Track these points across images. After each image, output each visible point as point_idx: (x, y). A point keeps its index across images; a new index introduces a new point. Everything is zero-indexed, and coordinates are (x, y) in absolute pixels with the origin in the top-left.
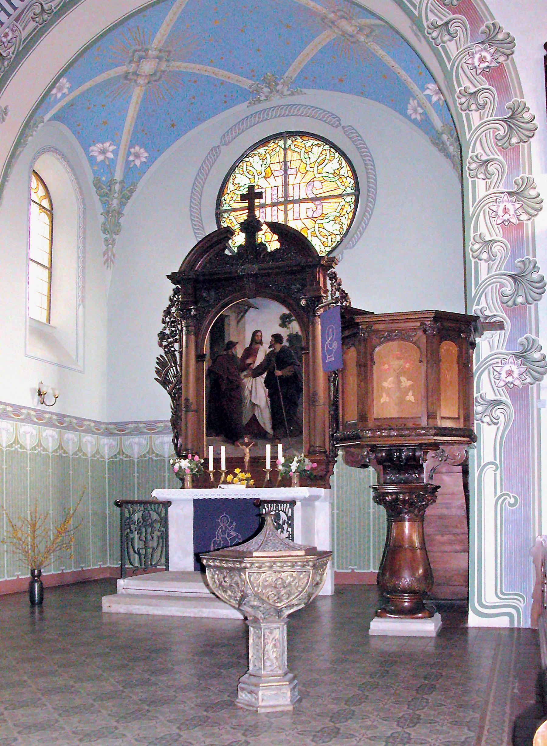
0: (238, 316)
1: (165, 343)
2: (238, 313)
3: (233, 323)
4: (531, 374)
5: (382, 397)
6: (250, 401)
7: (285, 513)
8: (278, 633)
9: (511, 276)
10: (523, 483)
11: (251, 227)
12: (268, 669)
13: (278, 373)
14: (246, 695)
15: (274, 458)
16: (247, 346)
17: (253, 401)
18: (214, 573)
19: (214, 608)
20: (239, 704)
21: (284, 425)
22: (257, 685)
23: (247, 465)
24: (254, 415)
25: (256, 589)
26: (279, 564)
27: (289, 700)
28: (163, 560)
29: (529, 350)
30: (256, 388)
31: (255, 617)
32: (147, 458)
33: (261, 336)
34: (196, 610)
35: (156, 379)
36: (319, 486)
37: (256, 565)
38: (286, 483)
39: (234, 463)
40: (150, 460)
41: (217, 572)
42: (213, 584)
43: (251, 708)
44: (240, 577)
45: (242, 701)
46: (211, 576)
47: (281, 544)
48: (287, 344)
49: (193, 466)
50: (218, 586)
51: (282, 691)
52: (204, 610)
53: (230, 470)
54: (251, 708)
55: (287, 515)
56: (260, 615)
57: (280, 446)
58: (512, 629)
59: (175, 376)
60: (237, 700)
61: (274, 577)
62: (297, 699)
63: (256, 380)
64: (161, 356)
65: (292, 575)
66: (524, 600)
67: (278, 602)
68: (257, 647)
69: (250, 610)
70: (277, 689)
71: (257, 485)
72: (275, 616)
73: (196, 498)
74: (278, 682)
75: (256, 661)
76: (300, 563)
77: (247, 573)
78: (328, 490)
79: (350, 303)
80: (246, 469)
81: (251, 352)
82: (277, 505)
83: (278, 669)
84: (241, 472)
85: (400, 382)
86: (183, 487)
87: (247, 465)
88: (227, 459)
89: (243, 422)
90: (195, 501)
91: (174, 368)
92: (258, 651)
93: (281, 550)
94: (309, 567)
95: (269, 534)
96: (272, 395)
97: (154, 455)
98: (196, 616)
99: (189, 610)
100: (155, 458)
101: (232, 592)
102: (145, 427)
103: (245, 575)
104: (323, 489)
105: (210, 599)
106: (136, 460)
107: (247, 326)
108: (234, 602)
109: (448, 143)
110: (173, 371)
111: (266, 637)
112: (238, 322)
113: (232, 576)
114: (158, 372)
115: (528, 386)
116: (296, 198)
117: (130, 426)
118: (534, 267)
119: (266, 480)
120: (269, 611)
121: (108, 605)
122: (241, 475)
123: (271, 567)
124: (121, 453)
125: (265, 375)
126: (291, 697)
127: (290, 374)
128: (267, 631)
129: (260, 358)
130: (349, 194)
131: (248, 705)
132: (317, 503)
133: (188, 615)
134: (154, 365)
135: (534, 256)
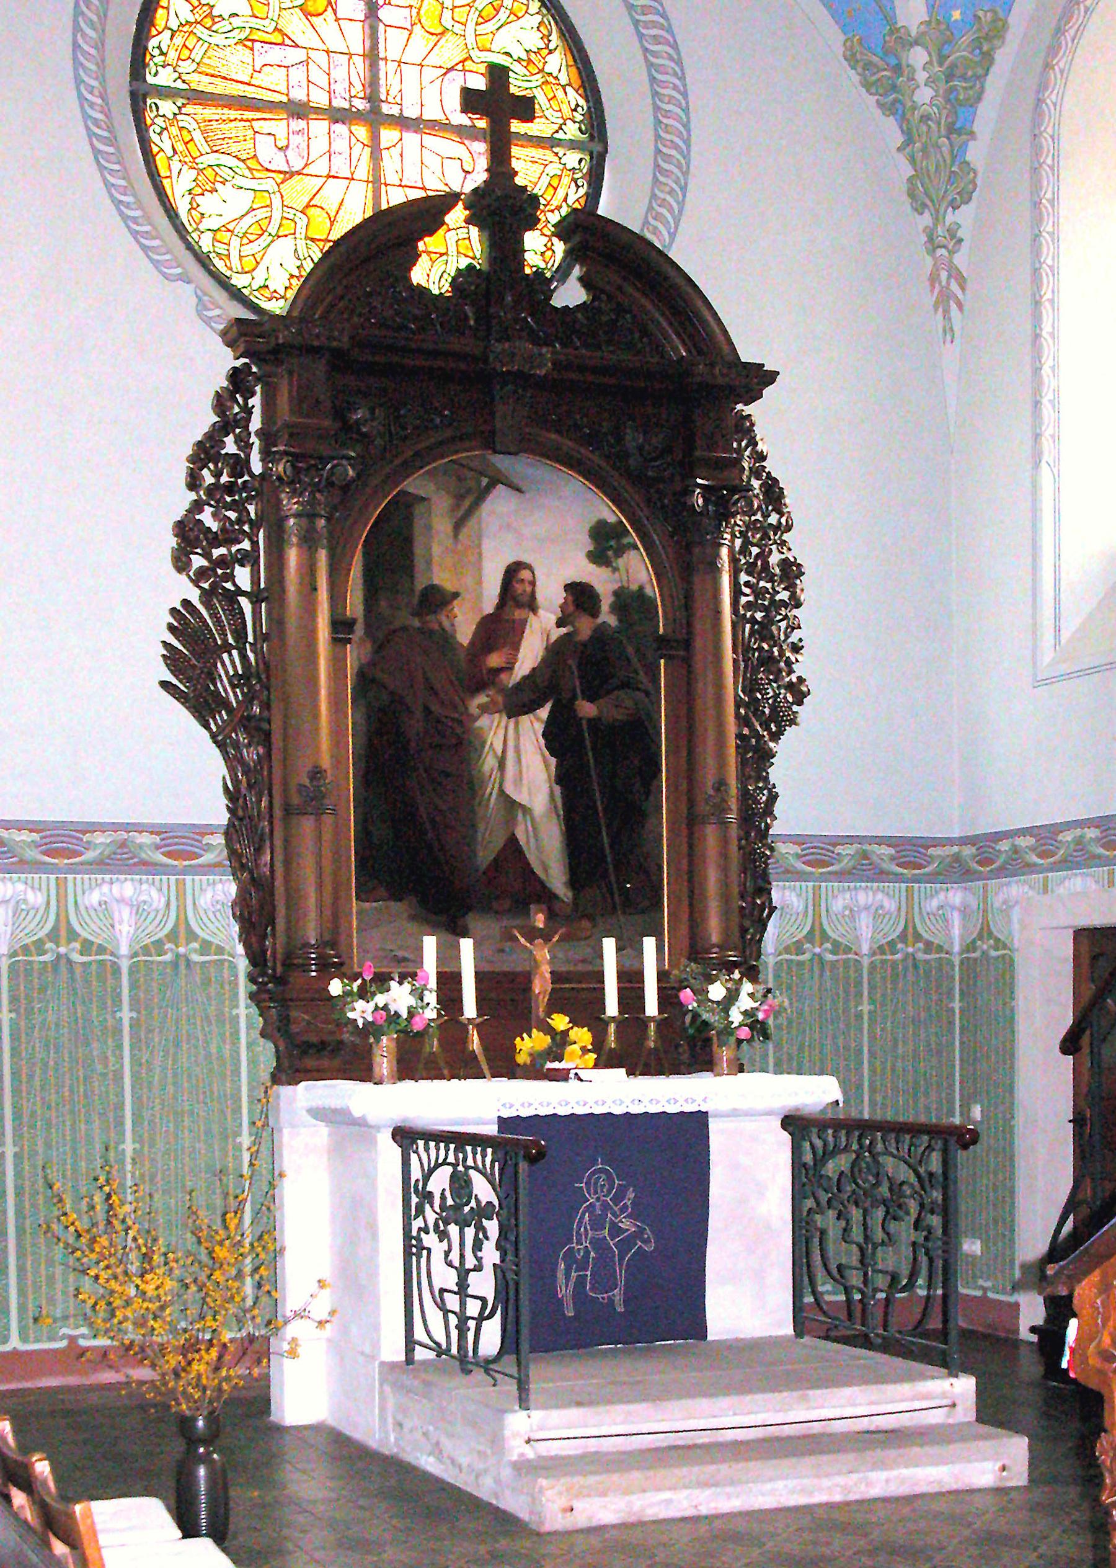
0: (455, 508)
1: (198, 562)
2: (459, 498)
3: (442, 524)
6: (501, 792)
11: (503, 209)
13: (587, 709)
15: (631, 981)
16: (489, 607)
17: (510, 790)
21: (605, 875)
24: (513, 841)
30: (517, 750)
32: (806, 957)
33: (533, 583)
35: (165, 685)
39: (506, 997)
40: (910, 963)
48: (612, 621)
52: (873, 1475)
57: (467, 946)
59: (236, 681)
63: (517, 724)
64: (186, 603)
79: (789, 517)
81: (500, 629)
88: (479, 976)
89: (479, 859)
91: (235, 653)
96: (569, 780)
97: (196, 945)
99: (826, 1482)
100: (76, 957)
102: (892, 858)
106: (866, 962)
107: (488, 546)
109: (921, 76)
110: (230, 663)
112: (458, 527)
114: (172, 659)
116: (411, 112)
117: (100, 838)
121: (563, 1502)
124: (63, 933)
125: (544, 713)
127: (619, 715)
129: (530, 655)
130: (573, 145)
134: (154, 633)
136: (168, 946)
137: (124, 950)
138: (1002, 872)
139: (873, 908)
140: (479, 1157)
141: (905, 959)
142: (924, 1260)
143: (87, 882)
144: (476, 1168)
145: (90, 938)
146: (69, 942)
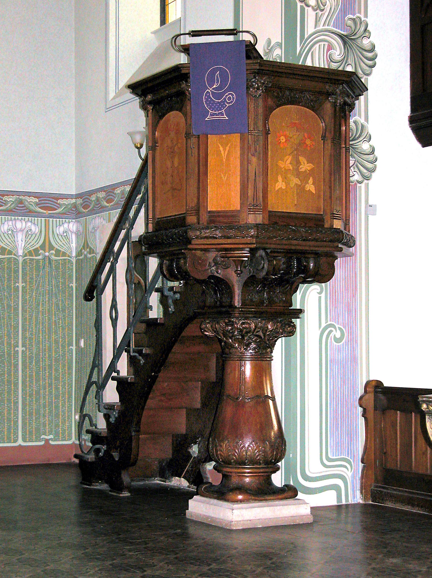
4: (359, 170)
5: (278, 181)
9: (341, 36)
10: (349, 311)
29: (360, 136)
58: (339, 507)
66: (351, 468)
85: (298, 163)
97: (53, 252)
100: (53, 257)
102: (37, 204)
106: (21, 260)
115: (356, 184)
117: (65, 202)
118: (365, 30)
135: (366, 16)
136: (41, 251)
137: (21, 252)
138: (93, 212)
139: (25, 231)
141: (44, 259)
143: (61, 221)
145: (5, 246)
146: (50, 250)
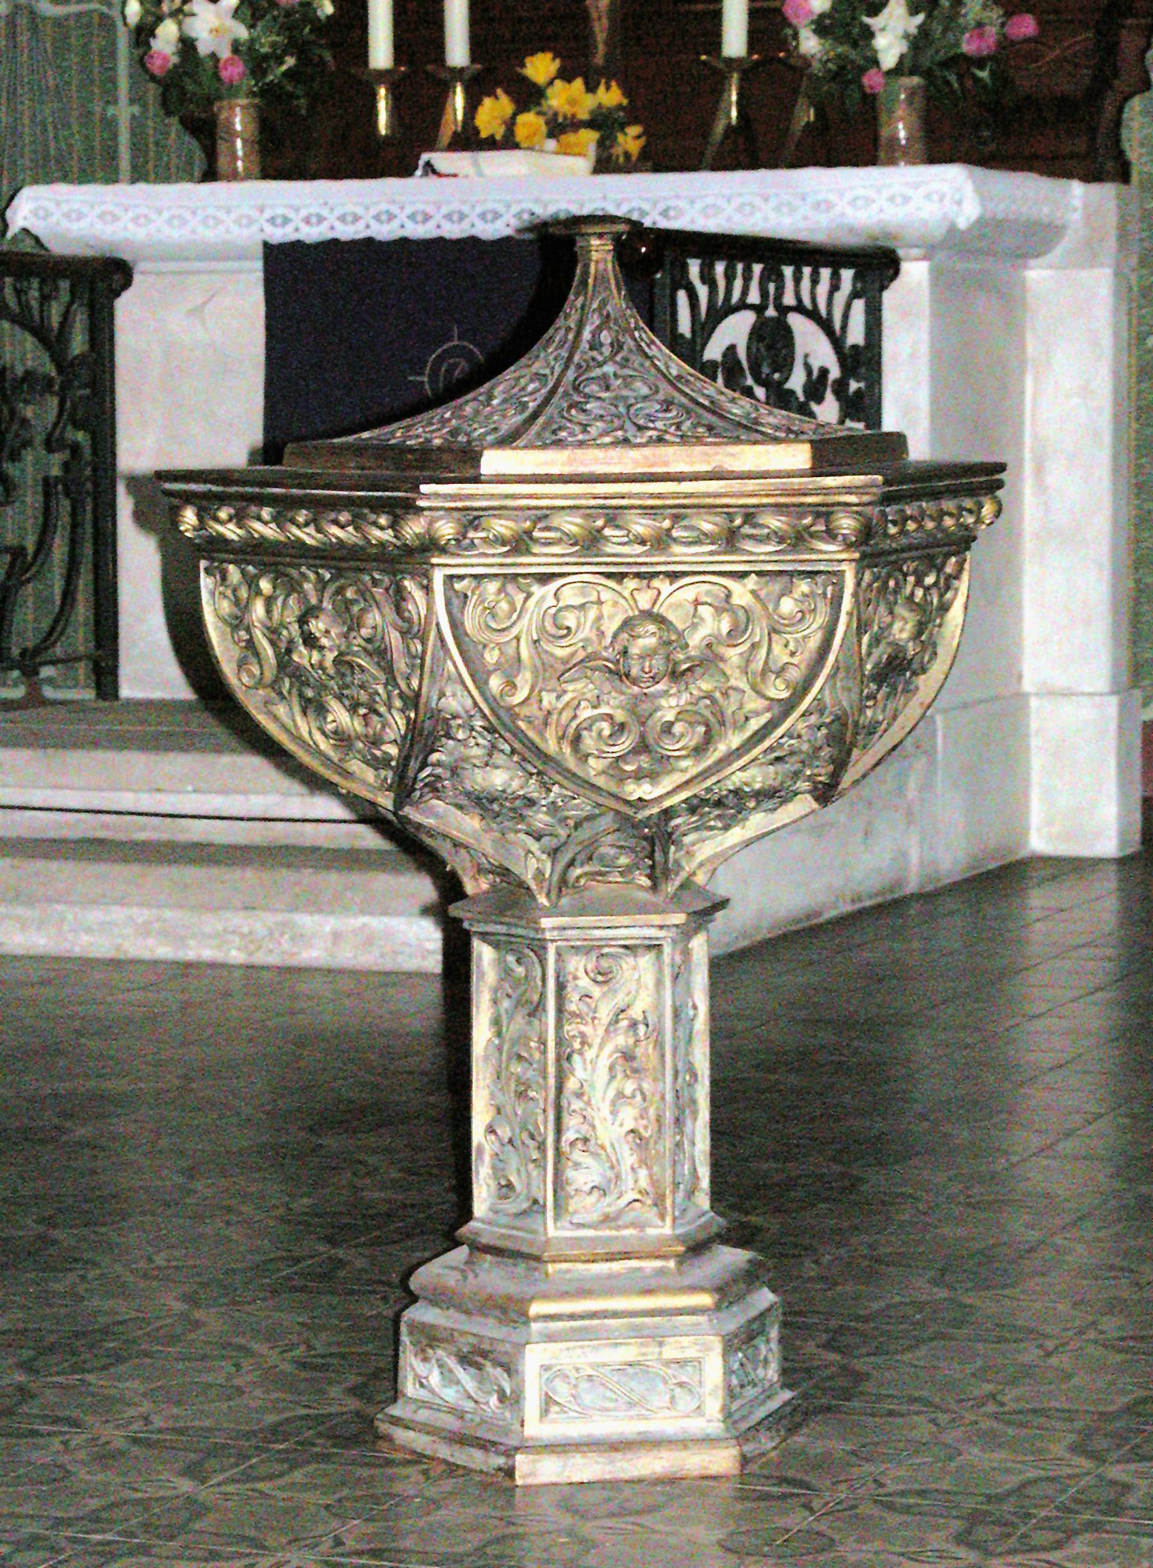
7: (825, 325)
8: (649, 979)
12: (587, 1207)
14: (449, 1378)
18: (244, 593)
19: (365, 909)
20: (401, 1435)
22: (512, 1311)
23: (600, 30)
25: (495, 683)
26: (641, 526)
27: (714, 1406)
28: (79, 635)
31: (504, 872)
34: (260, 923)
36: (1054, 165)
37: (501, 527)
38: (847, 139)
41: (265, 585)
42: (241, 664)
43: (474, 1458)
44: (399, 610)
45: (423, 1415)
46: (226, 606)
47: (667, 405)
49: (266, 42)
50: (269, 675)
51: (669, 1352)
52: (307, 921)
53: (495, 69)
54: (474, 1458)
55: (837, 342)
56: (532, 865)
60: (396, 1410)
61: (615, 605)
62: (773, 1405)
65: (725, 605)
67: (638, 776)
68: (517, 1068)
69: (467, 825)
70: (638, 1333)
71: (658, 158)
72: (626, 871)
73: (278, 235)
74: (648, 1292)
75: (513, 1161)
76: (775, 522)
77: (438, 576)
78: (1106, 193)
80: (599, 59)
82: (773, 274)
83: (651, 1214)
84: (566, 75)
86: (210, 175)
87: (600, 30)
90: (266, 245)
92: (522, 1095)
93: (660, 440)
94: (830, 548)
95: (595, 345)
98: (260, 958)
99: (212, 923)
101: (353, 709)
103: (427, 589)
104: (1077, 188)
105: (351, 859)
108: (370, 775)
111: (572, 1007)
113: (348, 604)
119: (719, 128)
120: (585, 833)
122: (568, 97)
123: (591, 542)
126: (731, 1394)
128: (577, 964)
131: (461, 1440)
132: (1037, 275)
133: (208, 954)
140: (806, 283)
142: (64, 505)
144: (800, 308)
